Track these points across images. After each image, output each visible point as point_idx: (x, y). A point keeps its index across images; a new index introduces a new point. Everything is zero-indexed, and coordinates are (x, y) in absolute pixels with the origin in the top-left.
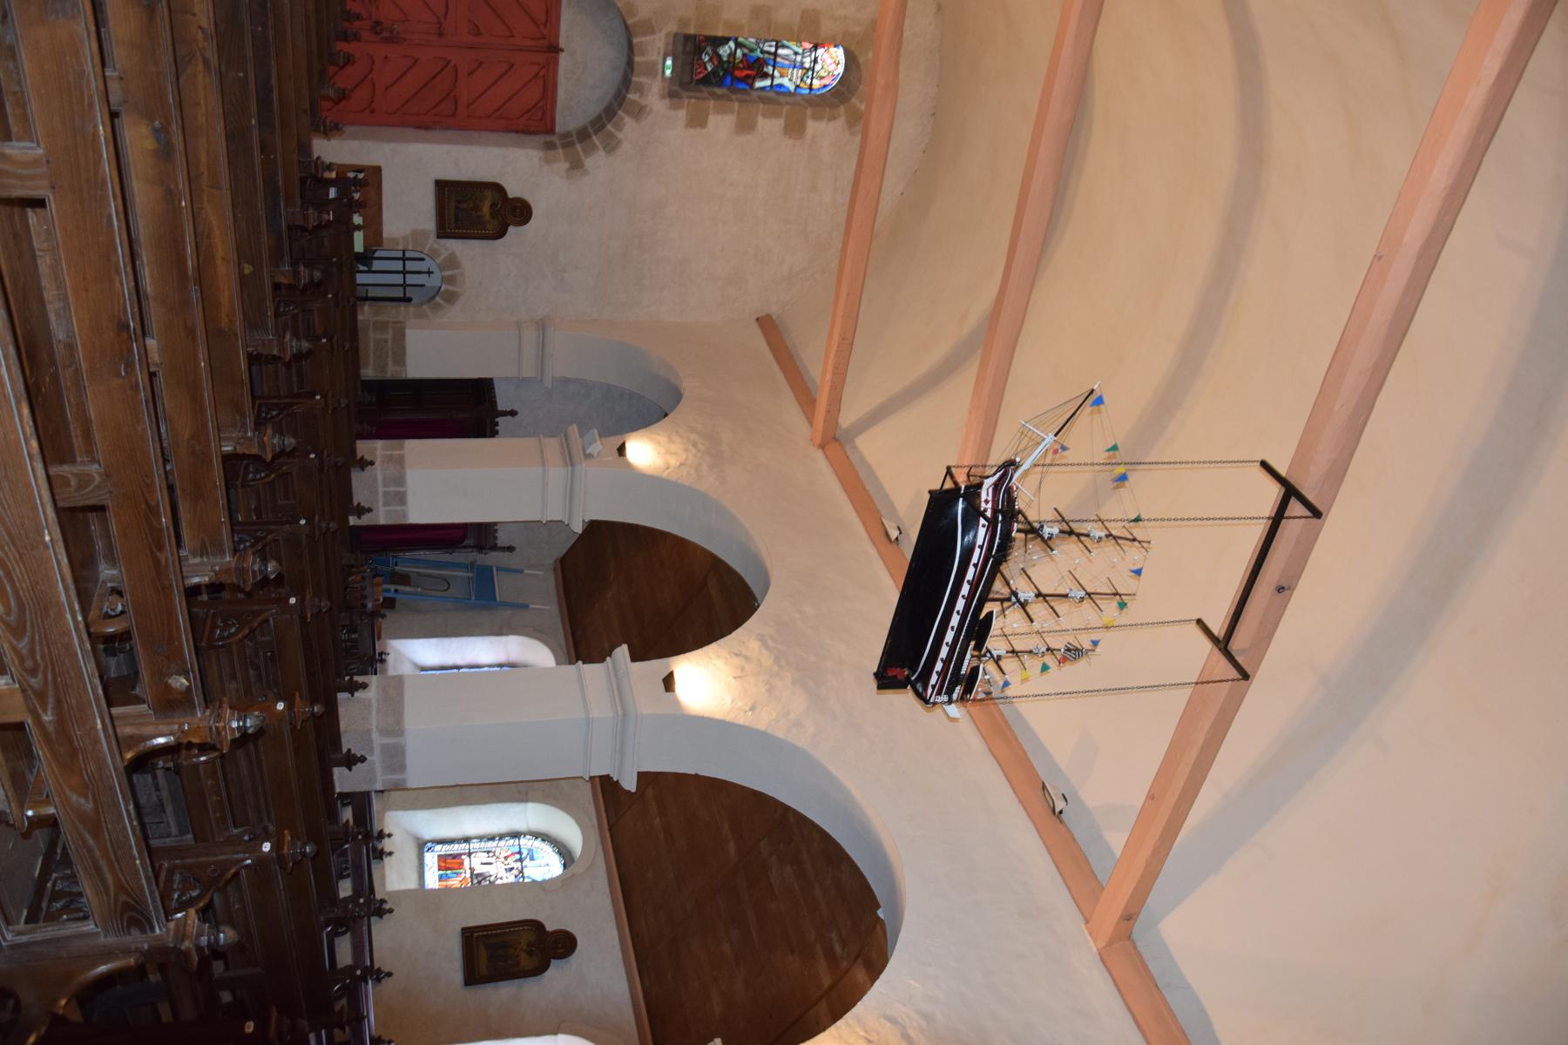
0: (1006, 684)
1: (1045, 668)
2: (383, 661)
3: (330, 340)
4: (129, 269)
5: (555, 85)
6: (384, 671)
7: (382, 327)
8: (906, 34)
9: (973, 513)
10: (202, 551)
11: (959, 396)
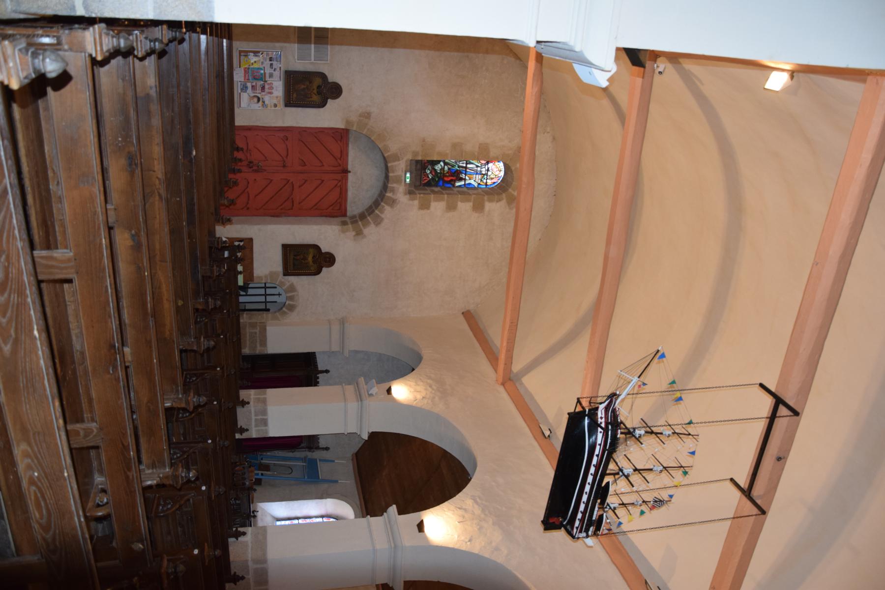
0: (620, 523)
1: (642, 513)
2: (255, 517)
3: (225, 336)
4: (116, 315)
5: (346, 190)
6: (255, 525)
7: (253, 325)
8: (537, 153)
9: (594, 425)
10: (153, 466)
11: (580, 352)
